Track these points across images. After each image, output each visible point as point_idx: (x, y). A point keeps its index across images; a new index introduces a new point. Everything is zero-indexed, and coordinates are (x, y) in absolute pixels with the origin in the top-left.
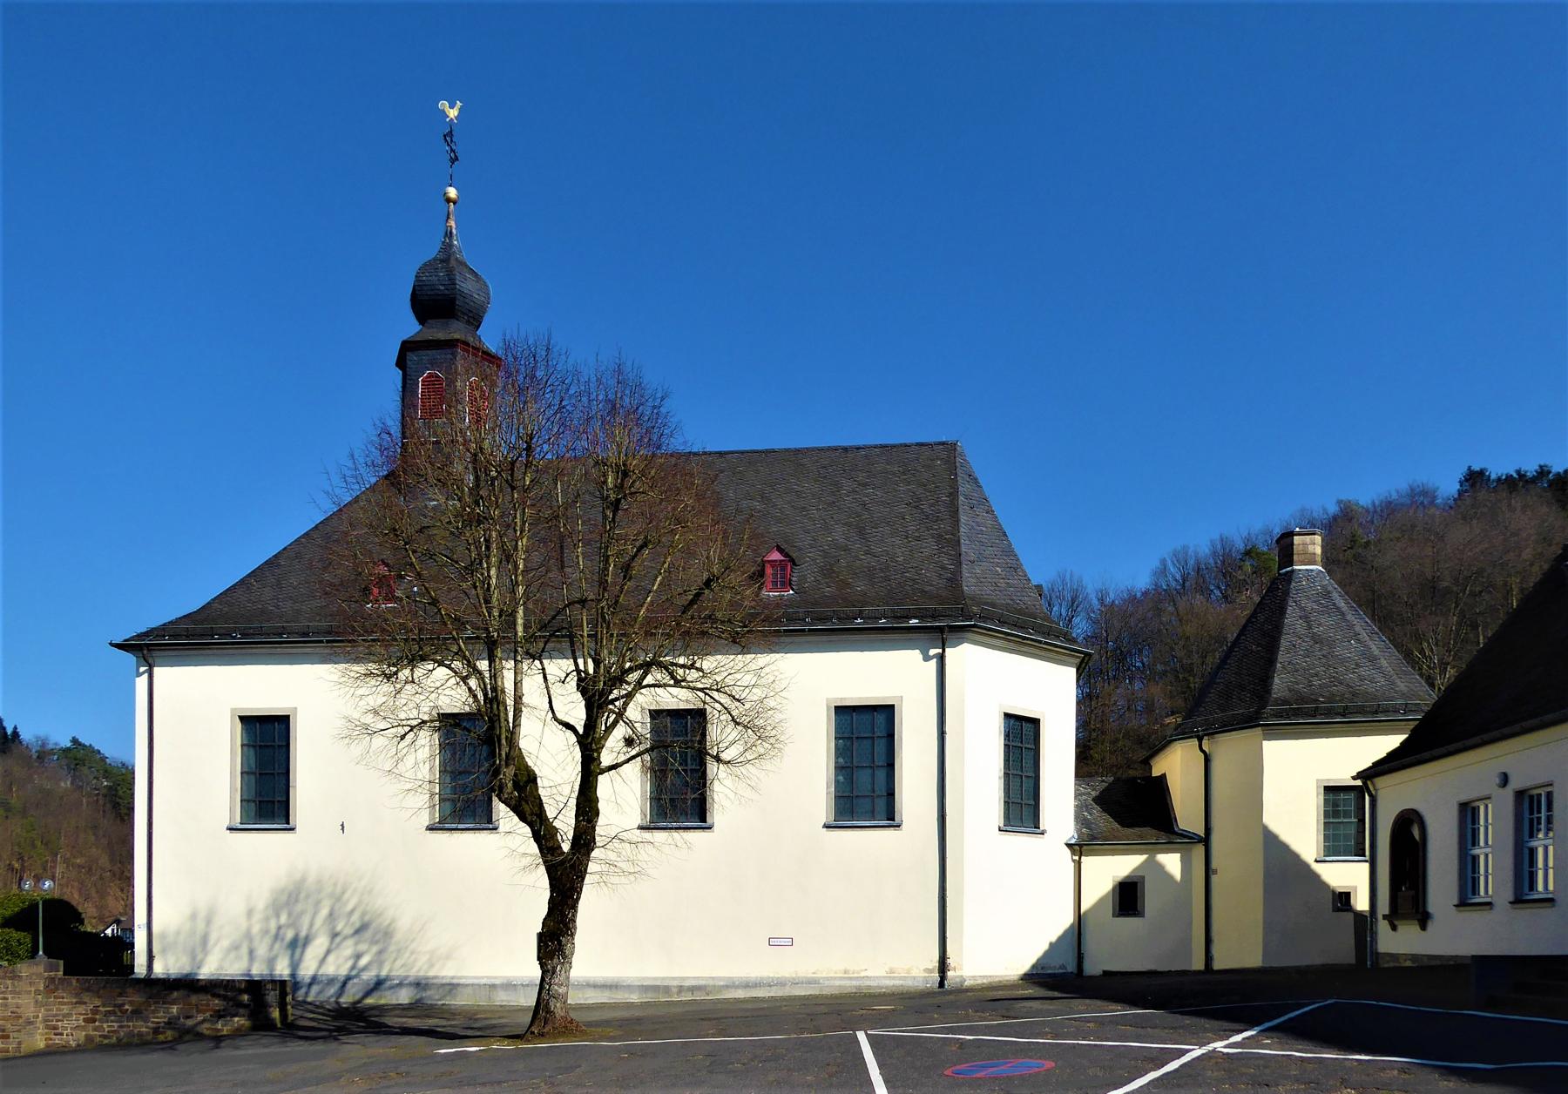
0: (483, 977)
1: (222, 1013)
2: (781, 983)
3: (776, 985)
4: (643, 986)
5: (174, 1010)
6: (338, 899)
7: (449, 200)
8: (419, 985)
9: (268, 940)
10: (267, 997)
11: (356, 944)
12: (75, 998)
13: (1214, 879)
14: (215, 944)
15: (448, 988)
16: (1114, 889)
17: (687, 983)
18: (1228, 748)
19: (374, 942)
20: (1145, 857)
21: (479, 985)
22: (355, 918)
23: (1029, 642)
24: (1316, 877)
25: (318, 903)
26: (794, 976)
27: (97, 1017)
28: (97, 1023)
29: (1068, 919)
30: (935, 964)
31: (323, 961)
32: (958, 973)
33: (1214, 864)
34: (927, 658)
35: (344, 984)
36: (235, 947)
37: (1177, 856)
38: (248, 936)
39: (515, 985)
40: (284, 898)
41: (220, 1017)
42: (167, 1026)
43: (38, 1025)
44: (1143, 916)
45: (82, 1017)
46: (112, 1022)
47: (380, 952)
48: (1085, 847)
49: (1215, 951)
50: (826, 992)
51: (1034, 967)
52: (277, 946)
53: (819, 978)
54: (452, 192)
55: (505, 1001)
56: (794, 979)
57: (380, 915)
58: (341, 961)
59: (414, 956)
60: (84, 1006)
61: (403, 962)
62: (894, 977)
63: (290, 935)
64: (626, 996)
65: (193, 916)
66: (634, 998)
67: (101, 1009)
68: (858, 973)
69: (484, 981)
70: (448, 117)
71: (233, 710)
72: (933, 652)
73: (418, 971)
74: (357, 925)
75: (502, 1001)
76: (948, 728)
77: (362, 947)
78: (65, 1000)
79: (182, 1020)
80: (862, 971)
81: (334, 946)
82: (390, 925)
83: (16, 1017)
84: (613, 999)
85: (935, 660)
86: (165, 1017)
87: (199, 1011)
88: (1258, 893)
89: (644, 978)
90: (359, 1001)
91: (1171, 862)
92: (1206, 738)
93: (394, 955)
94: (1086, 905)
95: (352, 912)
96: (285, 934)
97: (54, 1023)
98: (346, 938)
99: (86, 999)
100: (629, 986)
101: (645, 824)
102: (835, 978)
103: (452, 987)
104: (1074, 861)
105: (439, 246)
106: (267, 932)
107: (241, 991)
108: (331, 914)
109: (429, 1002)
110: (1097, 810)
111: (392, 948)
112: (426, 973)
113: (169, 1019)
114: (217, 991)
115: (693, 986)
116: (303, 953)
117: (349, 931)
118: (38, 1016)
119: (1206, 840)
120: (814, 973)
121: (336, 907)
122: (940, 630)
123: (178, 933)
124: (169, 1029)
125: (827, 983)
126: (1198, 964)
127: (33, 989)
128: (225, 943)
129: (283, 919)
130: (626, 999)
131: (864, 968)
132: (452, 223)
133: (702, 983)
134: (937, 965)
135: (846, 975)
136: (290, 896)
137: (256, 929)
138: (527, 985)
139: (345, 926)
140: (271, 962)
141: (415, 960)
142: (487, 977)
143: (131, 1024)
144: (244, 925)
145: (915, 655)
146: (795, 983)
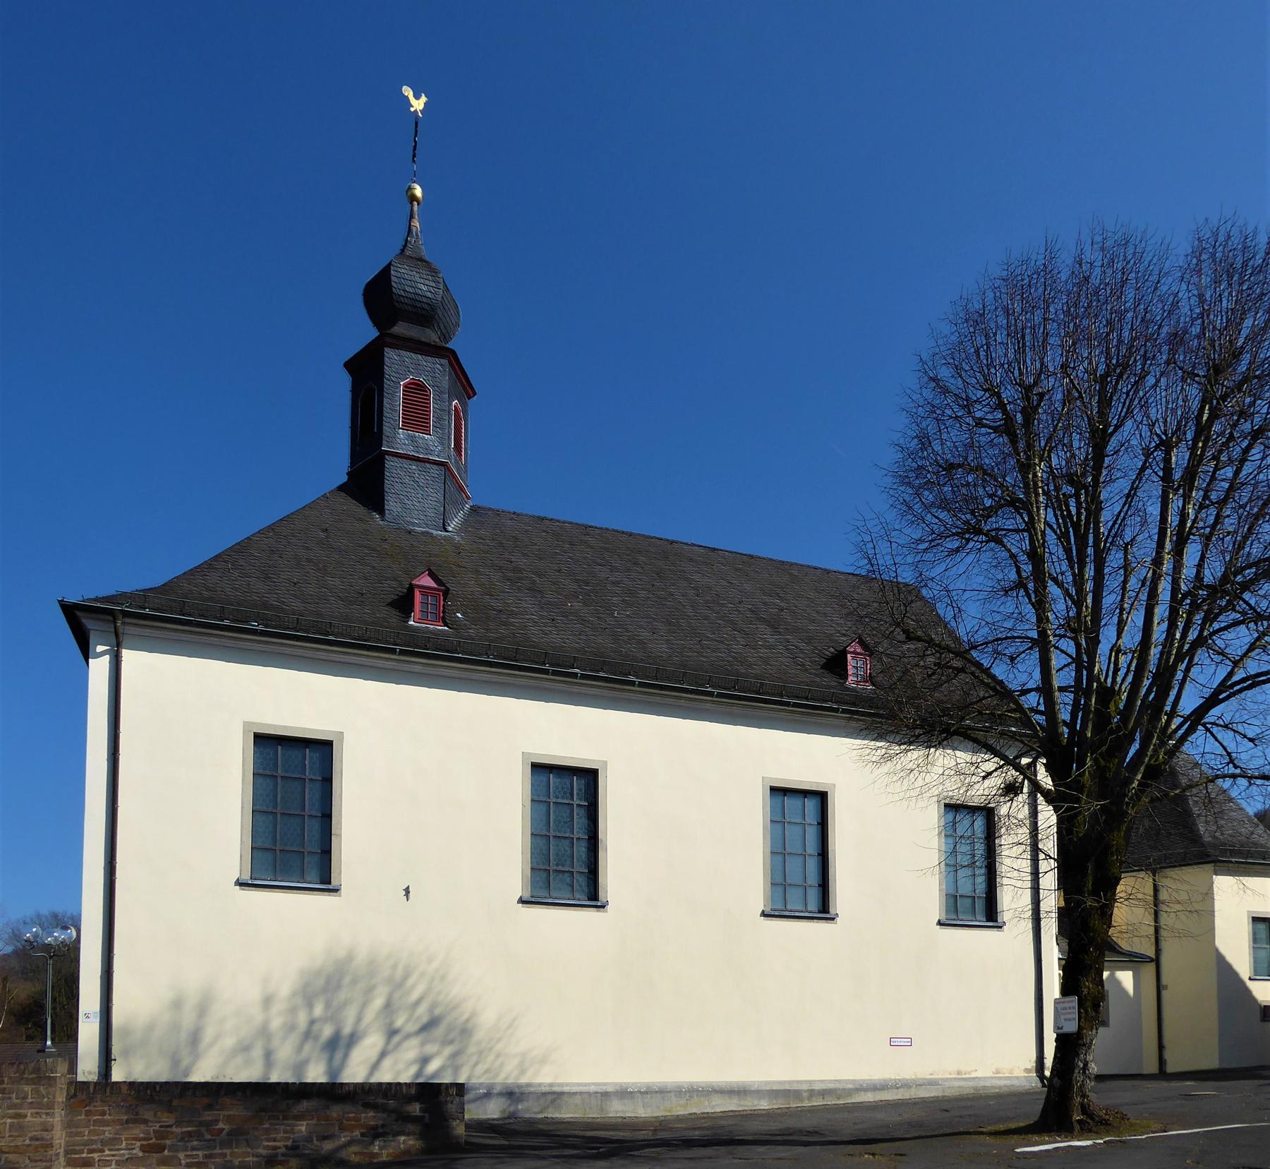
0: (589, 1084)
1: (381, 1130)
2: (906, 1085)
3: (902, 1087)
5: (303, 1127)
6: (398, 985)
7: (413, 198)
8: (512, 1094)
9: (293, 1039)
10: (449, 1106)
11: (423, 1044)
12: (126, 1114)
13: (1164, 993)
14: (211, 1045)
15: (550, 1097)
17: (817, 1087)
18: (1178, 883)
19: (446, 1042)
21: (589, 1093)
22: (422, 1010)
24: (1248, 992)
25: (369, 991)
26: (914, 1077)
27: (168, 1142)
28: (166, 1152)
31: (375, 1066)
36: (244, 1048)
37: (1104, 973)
38: (264, 1032)
39: (631, 1093)
40: (321, 982)
42: (290, 1152)
44: (1109, 1027)
45: (138, 1144)
46: (193, 1149)
47: (455, 1055)
49: (1167, 1055)
50: (948, 1093)
52: (307, 1047)
54: (418, 192)
57: (455, 1008)
58: (401, 1066)
59: (500, 1060)
60: (142, 1126)
61: (486, 1067)
63: (327, 1031)
64: (755, 1103)
65: (177, 1004)
66: (764, 1105)
67: (174, 1129)
69: (592, 1089)
71: (246, 725)
73: (506, 1078)
74: (425, 1020)
75: (617, 1112)
77: (430, 1049)
78: (107, 1117)
79: (315, 1142)
80: (972, 1071)
81: (391, 1047)
82: (467, 1021)
83: (42, 1146)
84: (741, 1106)
86: (288, 1139)
87: (342, 1129)
88: (1214, 1003)
93: (474, 1058)
95: (418, 1003)
96: (321, 1030)
97: (84, 1155)
98: (408, 1036)
102: (951, 1079)
103: (555, 1096)
106: (291, 1028)
107: (410, 1099)
109: (527, 1116)
111: (472, 1049)
113: (294, 1141)
114: (371, 1099)
115: (824, 1090)
116: (346, 1056)
117: (412, 1027)
119: (1157, 961)
120: (932, 1074)
121: (397, 995)
123: (150, 1028)
125: (947, 1084)
128: (229, 1042)
129: (318, 1010)
130: (756, 1106)
133: (831, 1086)
134: (1035, 1065)
135: (959, 1076)
136: (328, 980)
137: (276, 1023)
138: (646, 1093)
139: (407, 1021)
140: (300, 1067)
141: (502, 1065)
142: (594, 1084)
143: (228, 1151)
144: (259, 1018)
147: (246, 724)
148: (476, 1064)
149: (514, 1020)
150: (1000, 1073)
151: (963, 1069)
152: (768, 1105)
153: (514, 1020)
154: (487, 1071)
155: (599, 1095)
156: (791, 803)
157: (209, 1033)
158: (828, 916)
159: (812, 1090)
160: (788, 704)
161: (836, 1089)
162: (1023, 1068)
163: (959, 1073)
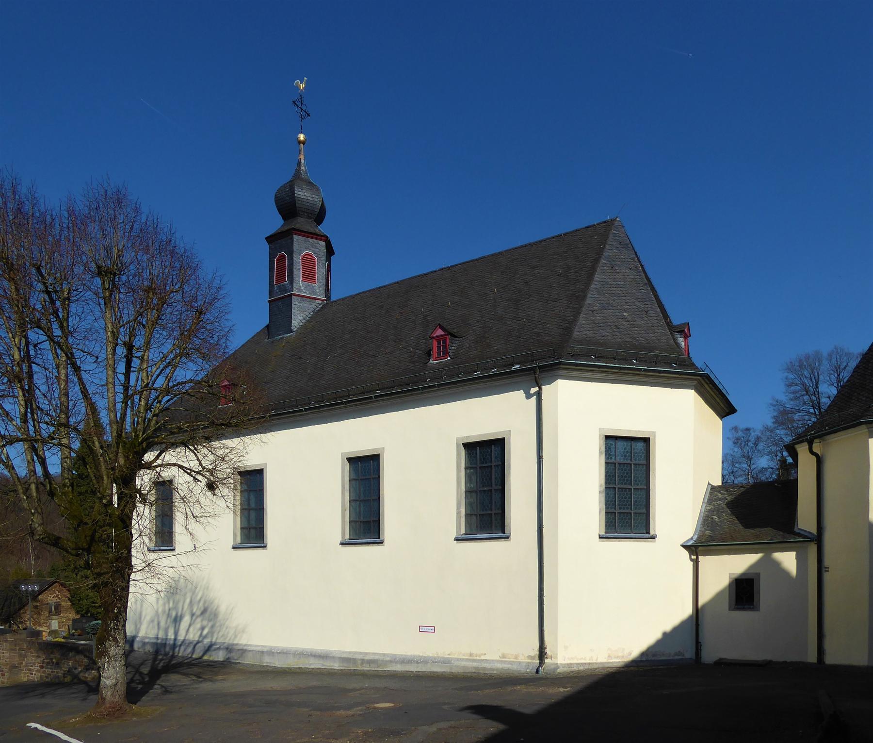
3: (421, 662)
4: (341, 657)
7: (300, 142)
8: (229, 649)
9: (165, 617)
11: (202, 621)
13: (827, 577)
14: (144, 620)
15: (241, 652)
16: (730, 585)
17: (367, 658)
19: (210, 620)
20: (759, 556)
23: (626, 371)
25: (185, 595)
29: (687, 611)
30: (536, 652)
32: (554, 661)
33: (827, 562)
34: (528, 396)
35: (195, 646)
41: (87, 670)
43: (22, 668)
47: (212, 627)
48: (700, 548)
50: (455, 670)
51: (643, 654)
53: (452, 659)
54: (302, 137)
55: (269, 663)
56: (435, 658)
57: (212, 603)
59: (228, 630)
61: (222, 633)
62: (506, 661)
64: (332, 664)
68: (480, 656)
70: (299, 89)
71: (654, 433)
72: (534, 390)
73: (230, 640)
75: (267, 662)
76: (544, 454)
77: (205, 623)
78: (33, 654)
82: (216, 610)
84: (324, 665)
85: (535, 397)
89: (344, 652)
90: (201, 658)
91: (788, 560)
92: (816, 441)
94: (702, 601)
96: (172, 613)
98: (197, 617)
99: (40, 655)
100: (333, 657)
101: (344, 541)
104: (692, 560)
105: (293, 172)
106: (164, 612)
108: (191, 602)
110: (726, 515)
111: (218, 624)
112: (233, 641)
117: (199, 613)
118: (22, 663)
119: (818, 539)
120: (449, 655)
122: (532, 370)
124: (69, 675)
125: (456, 663)
126: (812, 658)
127: (18, 648)
128: (148, 618)
130: (332, 666)
131: (484, 653)
132: (302, 157)
133: (376, 657)
137: (160, 610)
138: (280, 653)
139: (197, 609)
140: (166, 631)
141: (228, 633)
145: (520, 394)
146: (435, 661)
147: (266, 464)
148: (219, 632)
149: (232, 609)
150: (505, 658)
151: (474, 651)
152: (338, 667)
153: (232, 609)
154: (223, 635)
155: (260, 653)
156: (620, 444)
157: (144, 614)
158: (378, 540)
159: (363, 660)
160: (341, 403)
161: (377, 660)
162: (527, 655)
163: (471, 655)
